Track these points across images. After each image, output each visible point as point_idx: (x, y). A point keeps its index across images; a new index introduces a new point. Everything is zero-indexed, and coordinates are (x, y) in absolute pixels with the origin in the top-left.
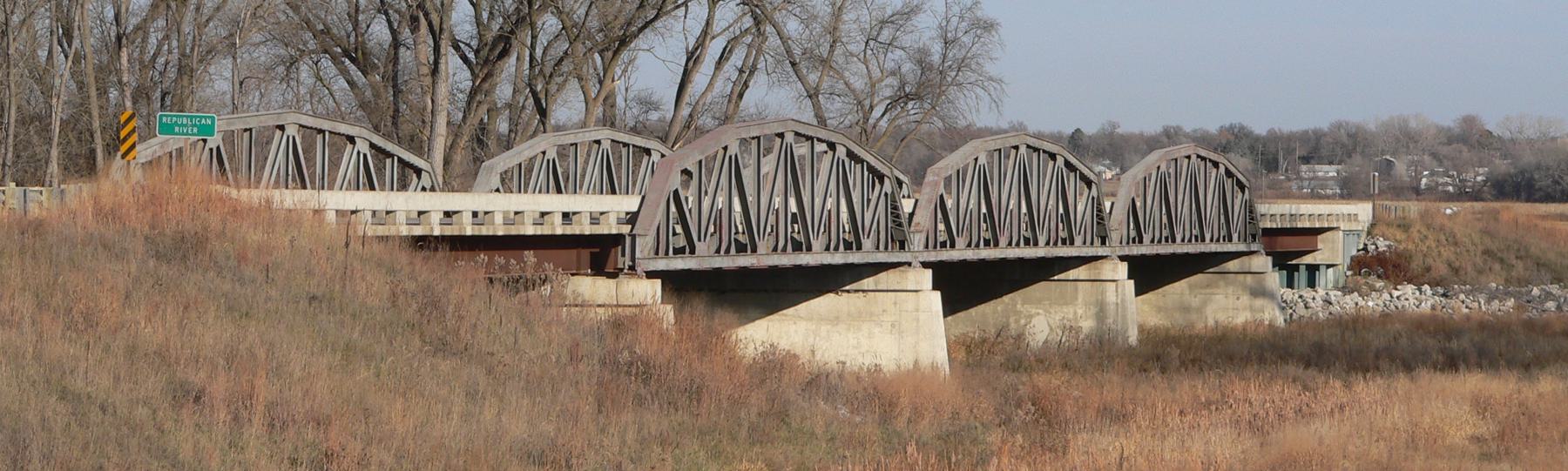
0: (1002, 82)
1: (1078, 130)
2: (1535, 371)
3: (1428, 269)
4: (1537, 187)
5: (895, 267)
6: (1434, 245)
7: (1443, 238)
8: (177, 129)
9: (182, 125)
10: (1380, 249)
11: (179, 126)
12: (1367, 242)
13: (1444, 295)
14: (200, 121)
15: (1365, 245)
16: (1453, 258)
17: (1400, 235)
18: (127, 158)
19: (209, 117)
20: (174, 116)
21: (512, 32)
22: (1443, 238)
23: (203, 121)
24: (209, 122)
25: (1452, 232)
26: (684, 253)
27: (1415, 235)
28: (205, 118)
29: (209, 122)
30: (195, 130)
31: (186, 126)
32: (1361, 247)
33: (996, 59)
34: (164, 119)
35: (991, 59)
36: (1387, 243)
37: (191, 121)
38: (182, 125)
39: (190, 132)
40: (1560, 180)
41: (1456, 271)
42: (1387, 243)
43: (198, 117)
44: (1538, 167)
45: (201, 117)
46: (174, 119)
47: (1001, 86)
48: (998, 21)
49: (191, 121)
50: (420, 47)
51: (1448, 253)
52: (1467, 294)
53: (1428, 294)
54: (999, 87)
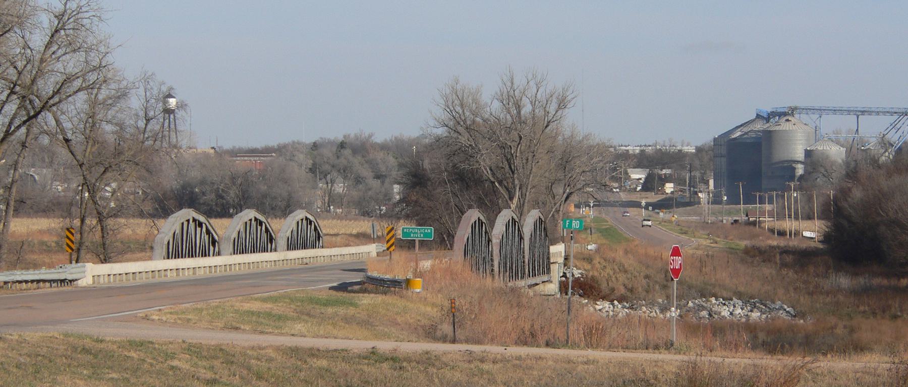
2: (865, 351)
3: (613, 290)
4: (201, 201)
6: (611, 273)
7: (616, 268)
8: (412, 235)
9: (415, 233)
10: (576, 276)
12: (565, 271)
13: (631, 308)
14: (424, 231)
15: (564, 273)
16: (626, 282)
17: (588, 267)
18: (390, 250)
22: (616, 268)
23: (426, 231)
24: (429, 231)
25: (621, 264)
27: (598, 265)
28: (427, 229)
29: (429, 231)
30: (422, 235)
31: (417, 233)
32: (562, 274)
36: (580, 271)
37: (420, 231)
38: (415, 233)
39: (419, 236)
40: (224, 194)
41: (631, 290)
42: (580, 271)
44: (203, 182)
45: (425, 229)
48: (186, 103)
49: (420, 231)
51: (622, 277)
52: (646, 306)
53: (619, 308)
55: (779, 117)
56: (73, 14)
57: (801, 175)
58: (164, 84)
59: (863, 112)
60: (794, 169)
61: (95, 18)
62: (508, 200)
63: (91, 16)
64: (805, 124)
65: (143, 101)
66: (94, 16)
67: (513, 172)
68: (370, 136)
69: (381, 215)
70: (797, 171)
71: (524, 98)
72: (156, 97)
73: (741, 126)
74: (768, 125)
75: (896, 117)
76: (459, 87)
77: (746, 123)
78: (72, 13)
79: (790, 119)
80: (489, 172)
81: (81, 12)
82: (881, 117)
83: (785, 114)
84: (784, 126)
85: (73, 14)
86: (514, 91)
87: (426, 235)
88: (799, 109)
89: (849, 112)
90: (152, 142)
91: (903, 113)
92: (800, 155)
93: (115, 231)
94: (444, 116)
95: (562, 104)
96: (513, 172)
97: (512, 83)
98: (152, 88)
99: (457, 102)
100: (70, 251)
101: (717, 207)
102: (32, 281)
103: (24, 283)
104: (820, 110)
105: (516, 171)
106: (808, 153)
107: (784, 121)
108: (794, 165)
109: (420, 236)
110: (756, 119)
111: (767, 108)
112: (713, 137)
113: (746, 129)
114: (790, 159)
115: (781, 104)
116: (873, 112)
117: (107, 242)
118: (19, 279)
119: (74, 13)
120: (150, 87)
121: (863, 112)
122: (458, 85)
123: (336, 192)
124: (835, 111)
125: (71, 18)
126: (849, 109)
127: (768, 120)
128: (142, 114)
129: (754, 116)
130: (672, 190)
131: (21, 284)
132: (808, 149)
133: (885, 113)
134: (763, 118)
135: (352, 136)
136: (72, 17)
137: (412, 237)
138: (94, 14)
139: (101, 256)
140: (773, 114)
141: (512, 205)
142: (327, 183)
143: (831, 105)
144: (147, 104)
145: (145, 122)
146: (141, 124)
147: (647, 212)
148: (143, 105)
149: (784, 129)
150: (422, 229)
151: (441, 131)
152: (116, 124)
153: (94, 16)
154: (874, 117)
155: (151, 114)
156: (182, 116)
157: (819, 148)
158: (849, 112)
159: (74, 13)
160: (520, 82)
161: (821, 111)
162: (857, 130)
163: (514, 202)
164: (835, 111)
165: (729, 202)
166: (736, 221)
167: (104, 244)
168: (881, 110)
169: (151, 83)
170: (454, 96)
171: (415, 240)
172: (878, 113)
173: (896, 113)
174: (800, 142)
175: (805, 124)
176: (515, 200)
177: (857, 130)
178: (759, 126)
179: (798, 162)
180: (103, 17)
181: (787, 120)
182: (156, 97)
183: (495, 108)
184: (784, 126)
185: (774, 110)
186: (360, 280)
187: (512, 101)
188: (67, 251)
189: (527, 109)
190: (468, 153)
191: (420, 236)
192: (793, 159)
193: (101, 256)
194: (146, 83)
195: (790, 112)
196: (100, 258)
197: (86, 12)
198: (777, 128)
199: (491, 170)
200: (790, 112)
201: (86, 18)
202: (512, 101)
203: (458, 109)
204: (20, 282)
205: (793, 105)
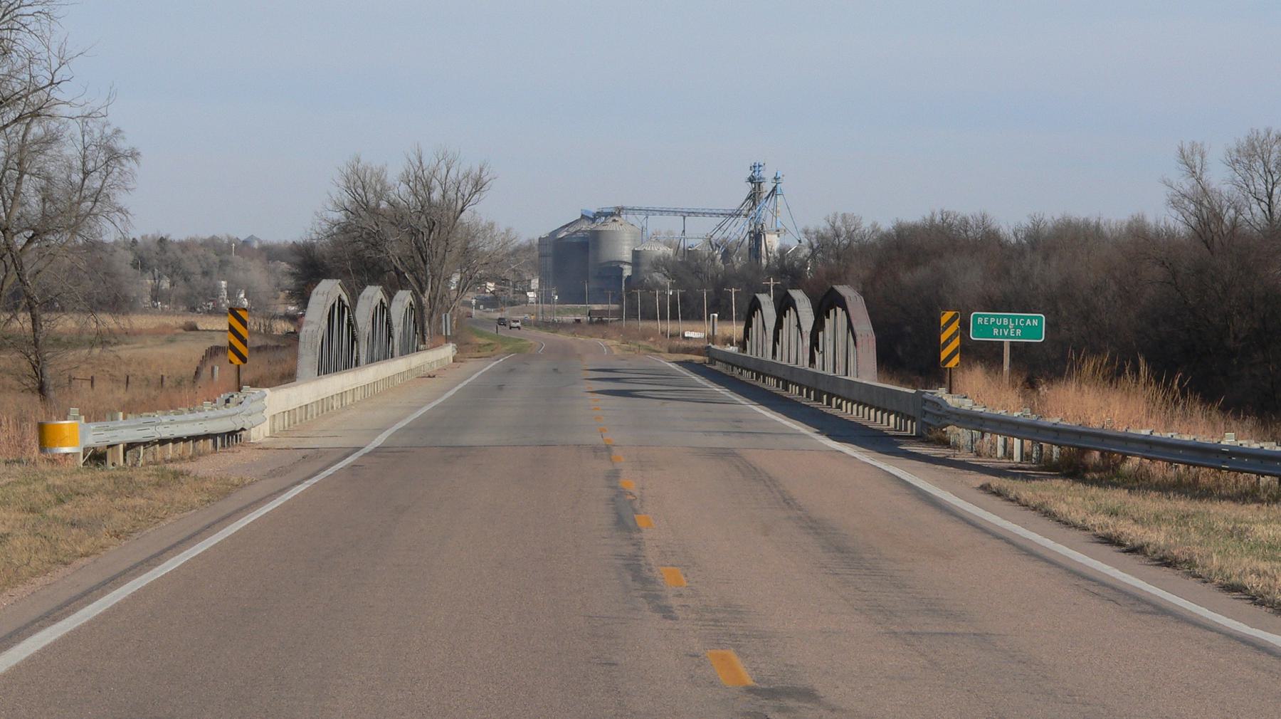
0: (128, 213)
1: (252, 235)
5: (851, 322)
8: (996, 331)
9: (1002, 327)
11: (999, 327)
19: (1035, 318)
20: (992, 316)
21: (7, 245)
23: (1028, 322)
26: (1013, 345)
29: (1035, 323)
30: (1019, 332)
33: (132, 190)
34: (980, 320)
35: (126, 189)
37: (1014, 322)
38: (1002, 327)
43: (1023, 317)
45: (1026, 318)
46: (992, 320)
47: (127, 217)
48: (139, 151)
49: (1014, 322)
50: (17, 467)
54: (125, 218)
55: (606, 217)
56: (10, 9)
57: (628, 276)
58: (109, 125)
59: (689, 214)
60: (622, 269)
61: (42, 15)
62: (419, 293)
63: (35, 13)
64: (632, 225)
65: (80, 148)
66: (40, 12)
67: (425, 262)
68: (168, 236)
69: (209, 311)
70: (625, 271)
71: (434, 180)
72: (97, 143)
73: (567, 226)
74: (594, 225)
75: (722, 219)
76: (360, 166)
77: (571, 223)
78: (9, 6)
79: (617, 219)
80: (398, 262)
81: (23, 6)
82: (708, 219)
83: (612, 214)
84: (611, 226)
85: (10, 9)
86: (423, 171)
87: (1027, 330)
88: (627, 209)
89: (675, 212)
90: (90, 204)
91: (730, 215)
92: (627, 255)
93: (53, 322)
94: (346, 199)
95: (478, 185)
96: (425, 262)
97: (421, 163)
98: (91, 131)
99: (359, 183)
100: (237, 361)
101: (546, 306)
102: (189, 438)
103: (158, 446)
104: (647, 210)
105: (428, 261)
106: (636, 254)
107: (611, 220)
108: (621, 266)
109: (1015, 333)
110: (580, 219)
111: (593, 209)
112: (539, 237)
113: (572, 230)
114: (617, 259)
115: (608, 204)
116: (699, 213)
117: (41, 337)
118: (165, 433)
119: (12, 7)
120: (89, 129)
121: (689, 214)
122: (359, 164)
123: (163, 288)
124: (661, 212)
125: (7, 14)
126: (676, 210)
127: (594, 220)
128: (77, 164)
129: (579, 217)
130: (494, 289)
131: (165, 446)
132: (636, 249)
133: (711, 214)
134: (588, 218)
135: (149, 236)
136: (9, 12)
137: (995, 337)
138: (41, 10)
139: (31, 357)
140: (599, 214)
141: (423, 298)
142: (155, 279)
143: (657, 206)
144: (85, 152)
145: (81, 176)
146: (77, 178)
147: (478, 311)
148: (80, 153)
149: (611, 229)
150: (1020, 317)
151: (339, 216)
152: (44, 178)
153: (40, 12)
154: (701, 218)
155: (91, 165)
156: (131, 169)
157: (646, 248)
158: (675, 212)
159: (12, 7)
160: (429, 162)
161: (648, 211)
162: (684, 231)
163: (426, 295)
164: (661, 212)
165: (559, 302)
166: (578, 321)
167: (36, 341)
168: (707, 211)
169: (91, 124)
170: (356, 177)
171: (1003, 342)
172: (704, 214)
173: (722, 214)
174: (627, 242)
175: (632, 225)
176: (427, 293)
177: (684, 231)
178: (585, 226)
179: (626, 263)
180: (54, 13)
181: (614, 221)
182: (97, 143)
183: (401, 192)
184: (611, 226)
185: (600, 211)
186: (1227, 450)
187: (420, 183)
188: (231, 362)
189: (436, 196)
190: (375, 241)
191: (1015, 333)
192: (620, 259)
193: (31, 357)
194: (84, 124)
195: (617, 213)
196: (30, 359)
197: (30, 5)
198: (604, 228)
199: (400, 259)
200: (617, 213)
201: (29, 15)
202: (420, 183)
203: (360, 191)
204: (163, 442)
205: (619, 205)
